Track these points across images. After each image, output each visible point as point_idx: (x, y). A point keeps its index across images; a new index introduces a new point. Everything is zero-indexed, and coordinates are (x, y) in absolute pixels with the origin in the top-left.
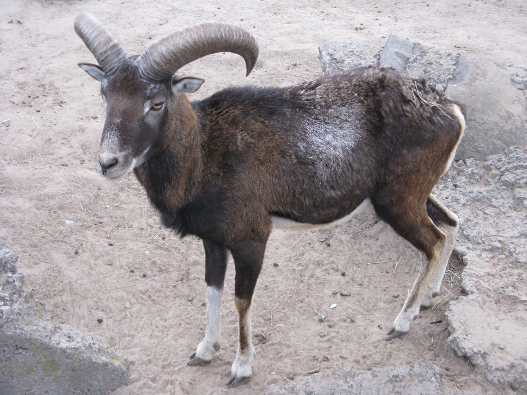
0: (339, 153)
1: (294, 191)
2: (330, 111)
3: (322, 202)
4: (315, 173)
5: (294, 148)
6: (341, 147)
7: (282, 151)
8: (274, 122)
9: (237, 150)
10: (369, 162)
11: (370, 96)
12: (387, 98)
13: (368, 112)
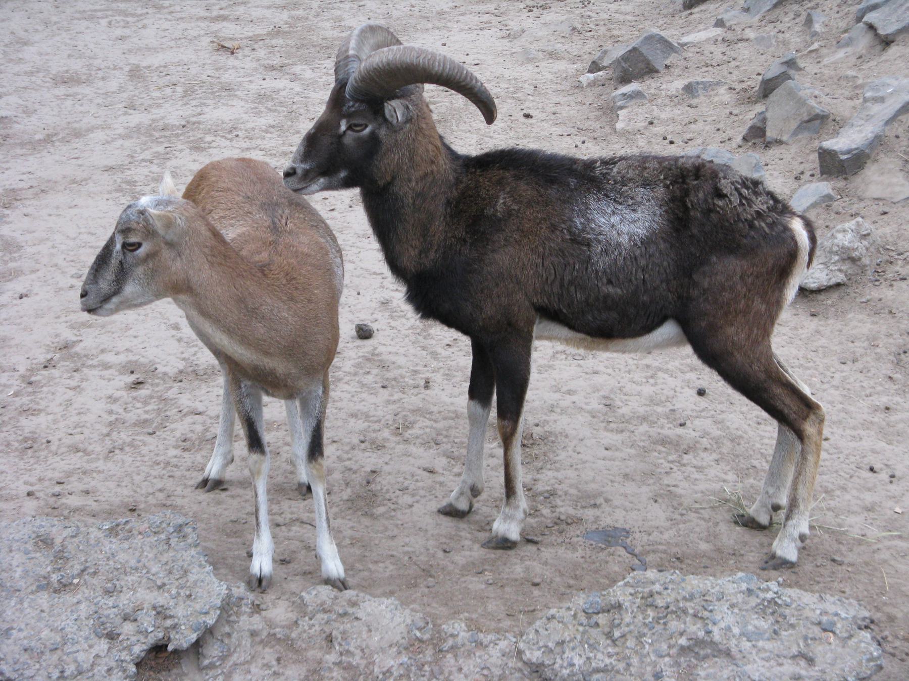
0: (624, 240)
1: (562, 279)
2: (624, 188)
3: (597, 299)
4: (589, 258)
5: (569, 223)
6: (628, 234)
7: (552, 225)
8: (553, 192)
9: (495, 215)
10: (665, 264)
11: (678, 183)
12: (697, 189)
13: (673, 199)
